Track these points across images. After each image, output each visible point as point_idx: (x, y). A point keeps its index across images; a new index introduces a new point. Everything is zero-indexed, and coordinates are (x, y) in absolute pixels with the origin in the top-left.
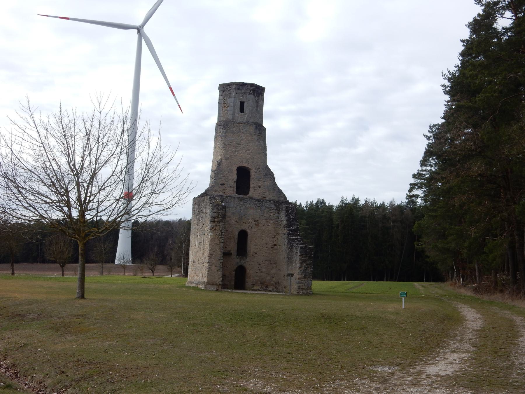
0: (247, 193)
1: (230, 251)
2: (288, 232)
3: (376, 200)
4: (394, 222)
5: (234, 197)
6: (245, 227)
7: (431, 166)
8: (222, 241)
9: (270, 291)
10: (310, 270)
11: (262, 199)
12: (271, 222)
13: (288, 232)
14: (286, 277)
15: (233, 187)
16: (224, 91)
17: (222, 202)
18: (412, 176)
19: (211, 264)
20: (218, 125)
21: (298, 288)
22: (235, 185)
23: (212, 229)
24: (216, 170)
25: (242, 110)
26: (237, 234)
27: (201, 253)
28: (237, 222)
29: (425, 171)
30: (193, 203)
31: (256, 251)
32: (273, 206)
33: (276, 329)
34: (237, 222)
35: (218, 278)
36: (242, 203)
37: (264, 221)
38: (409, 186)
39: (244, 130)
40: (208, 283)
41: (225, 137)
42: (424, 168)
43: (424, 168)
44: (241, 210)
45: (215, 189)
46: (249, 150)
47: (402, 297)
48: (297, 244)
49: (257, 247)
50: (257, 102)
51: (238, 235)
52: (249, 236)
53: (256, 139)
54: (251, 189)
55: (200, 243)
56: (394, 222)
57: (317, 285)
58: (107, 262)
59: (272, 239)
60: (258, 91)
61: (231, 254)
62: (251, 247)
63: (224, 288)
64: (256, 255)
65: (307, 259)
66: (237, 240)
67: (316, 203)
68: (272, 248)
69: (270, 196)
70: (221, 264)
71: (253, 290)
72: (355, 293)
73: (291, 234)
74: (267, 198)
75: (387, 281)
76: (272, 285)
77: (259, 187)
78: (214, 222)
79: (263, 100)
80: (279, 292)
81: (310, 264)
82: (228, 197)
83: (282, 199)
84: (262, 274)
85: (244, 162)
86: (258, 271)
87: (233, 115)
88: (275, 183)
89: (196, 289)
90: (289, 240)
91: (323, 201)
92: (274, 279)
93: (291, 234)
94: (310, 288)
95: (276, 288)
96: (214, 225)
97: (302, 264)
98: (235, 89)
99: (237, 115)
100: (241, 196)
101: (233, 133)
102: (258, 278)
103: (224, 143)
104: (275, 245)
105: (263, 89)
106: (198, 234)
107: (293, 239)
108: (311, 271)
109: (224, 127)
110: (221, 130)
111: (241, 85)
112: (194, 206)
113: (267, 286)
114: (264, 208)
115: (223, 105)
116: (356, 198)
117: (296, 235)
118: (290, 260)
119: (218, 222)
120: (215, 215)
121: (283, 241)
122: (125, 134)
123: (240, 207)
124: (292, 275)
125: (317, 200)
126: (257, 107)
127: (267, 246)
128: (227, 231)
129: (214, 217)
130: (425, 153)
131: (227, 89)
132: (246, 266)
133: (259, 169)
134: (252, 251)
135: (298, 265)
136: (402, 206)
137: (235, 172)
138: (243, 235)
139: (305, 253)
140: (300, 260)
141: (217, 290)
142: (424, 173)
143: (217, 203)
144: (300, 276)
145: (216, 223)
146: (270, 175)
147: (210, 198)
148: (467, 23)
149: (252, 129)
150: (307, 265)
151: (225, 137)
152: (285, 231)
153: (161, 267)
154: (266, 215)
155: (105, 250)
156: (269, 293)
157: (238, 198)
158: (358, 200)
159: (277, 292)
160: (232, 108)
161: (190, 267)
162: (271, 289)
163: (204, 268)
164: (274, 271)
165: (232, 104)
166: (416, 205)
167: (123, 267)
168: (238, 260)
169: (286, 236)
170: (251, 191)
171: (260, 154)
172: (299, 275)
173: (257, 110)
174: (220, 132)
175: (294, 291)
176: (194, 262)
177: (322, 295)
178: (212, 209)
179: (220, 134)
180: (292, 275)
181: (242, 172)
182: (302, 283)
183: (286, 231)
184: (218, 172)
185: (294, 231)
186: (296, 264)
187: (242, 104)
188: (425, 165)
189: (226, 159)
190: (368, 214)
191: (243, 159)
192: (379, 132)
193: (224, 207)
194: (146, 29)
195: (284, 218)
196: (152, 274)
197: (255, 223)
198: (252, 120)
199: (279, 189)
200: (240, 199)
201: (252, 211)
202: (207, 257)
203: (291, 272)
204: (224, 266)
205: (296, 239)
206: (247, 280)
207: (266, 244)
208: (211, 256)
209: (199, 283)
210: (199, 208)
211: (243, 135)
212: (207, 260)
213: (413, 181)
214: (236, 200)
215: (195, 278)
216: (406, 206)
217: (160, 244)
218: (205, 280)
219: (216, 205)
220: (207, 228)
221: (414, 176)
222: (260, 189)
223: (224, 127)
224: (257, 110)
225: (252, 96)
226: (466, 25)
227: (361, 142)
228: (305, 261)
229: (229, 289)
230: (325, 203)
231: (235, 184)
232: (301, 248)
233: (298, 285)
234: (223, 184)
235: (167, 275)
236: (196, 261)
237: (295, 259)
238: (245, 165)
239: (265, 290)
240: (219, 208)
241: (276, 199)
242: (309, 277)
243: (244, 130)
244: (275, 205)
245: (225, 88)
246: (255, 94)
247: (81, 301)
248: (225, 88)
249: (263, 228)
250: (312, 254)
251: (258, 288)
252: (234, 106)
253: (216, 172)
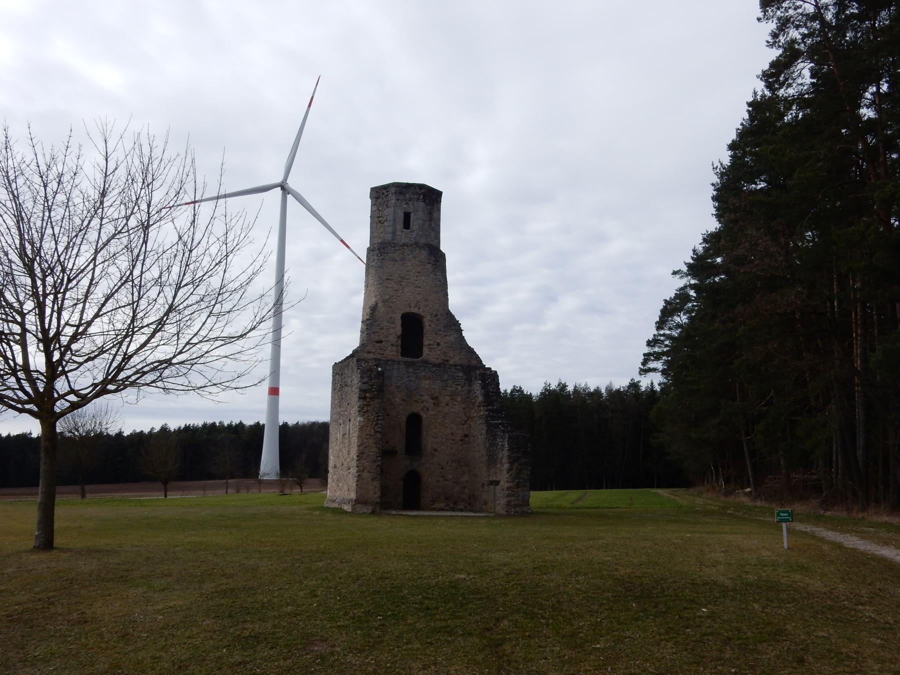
0: (420, 354)
3: (589, 385)
6: (416, 408)
7: (670, 329)
9: (461, 510)
12: (459, 399)
14: (486, 487)
16: (378, 198)
17: (378, 366)
18: (645, 343)
19: (361, 471)
21: (507, 505)
22: (400, 343)
23: (362, 411)
25: (407, 224)
26: (404, 419)
27: (345, 452)
28: (404, 400)
29: (664, 335)
32: (461, 374)
33: (507, 648)
34: (404, 400)
35: (374, 492)
36: (411, 370)
37: (448, 398)
39: (411, 256)
40: (358, 501)
41: (381, 267)
42: (662, 332)
43: (662, 332)
45: (367, 349)
47: (781, 521)
48: (503, 432)
51: (407, 422)
52: (425, 423)
54: (425, 349)
55: (344, 435)
57: (537, 498)
61: (396, 452)
62: (429, 441)
63: (386, 509)
66: (405, 430)
67: (512, 392)
69: (456, 358)
71: (433, 510)
72: (587, 508)
74: (451, 362)
77: (438, 344)
78: (365, 398)
79: (439, 210)
80: (476, 512)
82: (387, 361)
83: (474, 362)
85: (413, 305)
86: (441, 479)
87: (394, 233)
89: (339, 512)
90: (489, 426)
92: (466, 491)
94: (527, 503)
95: (470, 504)
96: (365, 403)
97: (511, 463)
98: (395, 193)
99: (400, 233)
100: (409, 360)
101: (394, 260)
104: (466, 436)
106: (341, 421)
109: (381, 253)
110: (375, 257)
112: (334, 376)
113: (455, 503)
115: (377, 220)
117: (499, 418)
118: (492, 460)
119: (371, 398)
120: (365, 387)
121: (479, 431)
123: (409, 377)
124: (497, 483)
128: (388, 415)
130: (662, 311)
134: (429, 446)
135: (506, 466)
138: (414, 422)
140: (509, 457)
141: (373, 512)
142: (662, 338)
148: (760, 73)
149: (424, 254)
151: (381, 267)
152: (482, 413)
153: (311, 481)
156: (460, 514)
157: (405, 362)
159: (472, 511)
160: (391, 223)
161: (330, 476)
162: (461, 507)
164: (465, 478)
165: (391, 217)
167: (270, 483)
170: (426, 351)
171: (437, 292)
172: (508, 482)
173: (430, 225)
175: (500, 509)
176: (335, 467)
177: (548, 514)
178: (361, 377)
180: (497, 483)
181: (409, 332)
184: (372, 322)
186: (502, 465)
187: (407, 216)
188: (662, 329)
189: (384, 301)
191: (410, 299)
192: (569, 302)
193: (381, 374)
194: (291, 183)
195: (478, 392)
198: (423, 241)
200: (408, 365)
201: (428, 382)
202: (355, 457)
205: (500, 424)
207: (452, 434)
208: (360, 456)
209: (343, 501)
211: (409, 264)
212: (354, 463)
213: (647, 350)
216: (627, 391)
217: (304, 448)
218: (353, 496)
219: (368, 371)
220: (354, 410)
221: (649, 343)
223: (380, 252)
224: (430, 225)
225: (422, 204)
226: (758, 77)
227: (575, 295)
229: (395, 509)
231: (400, 341)
232: (510, 438)
234: (381, 342)
236: (338, 465)
238: (415, 310)
239: (453, 510)
243: (411, 256)
245: (379, 194)
247: (44, 556)
248: (379, 194)
249: (447, 409)
251: (442, 505)
252: (394, 220)
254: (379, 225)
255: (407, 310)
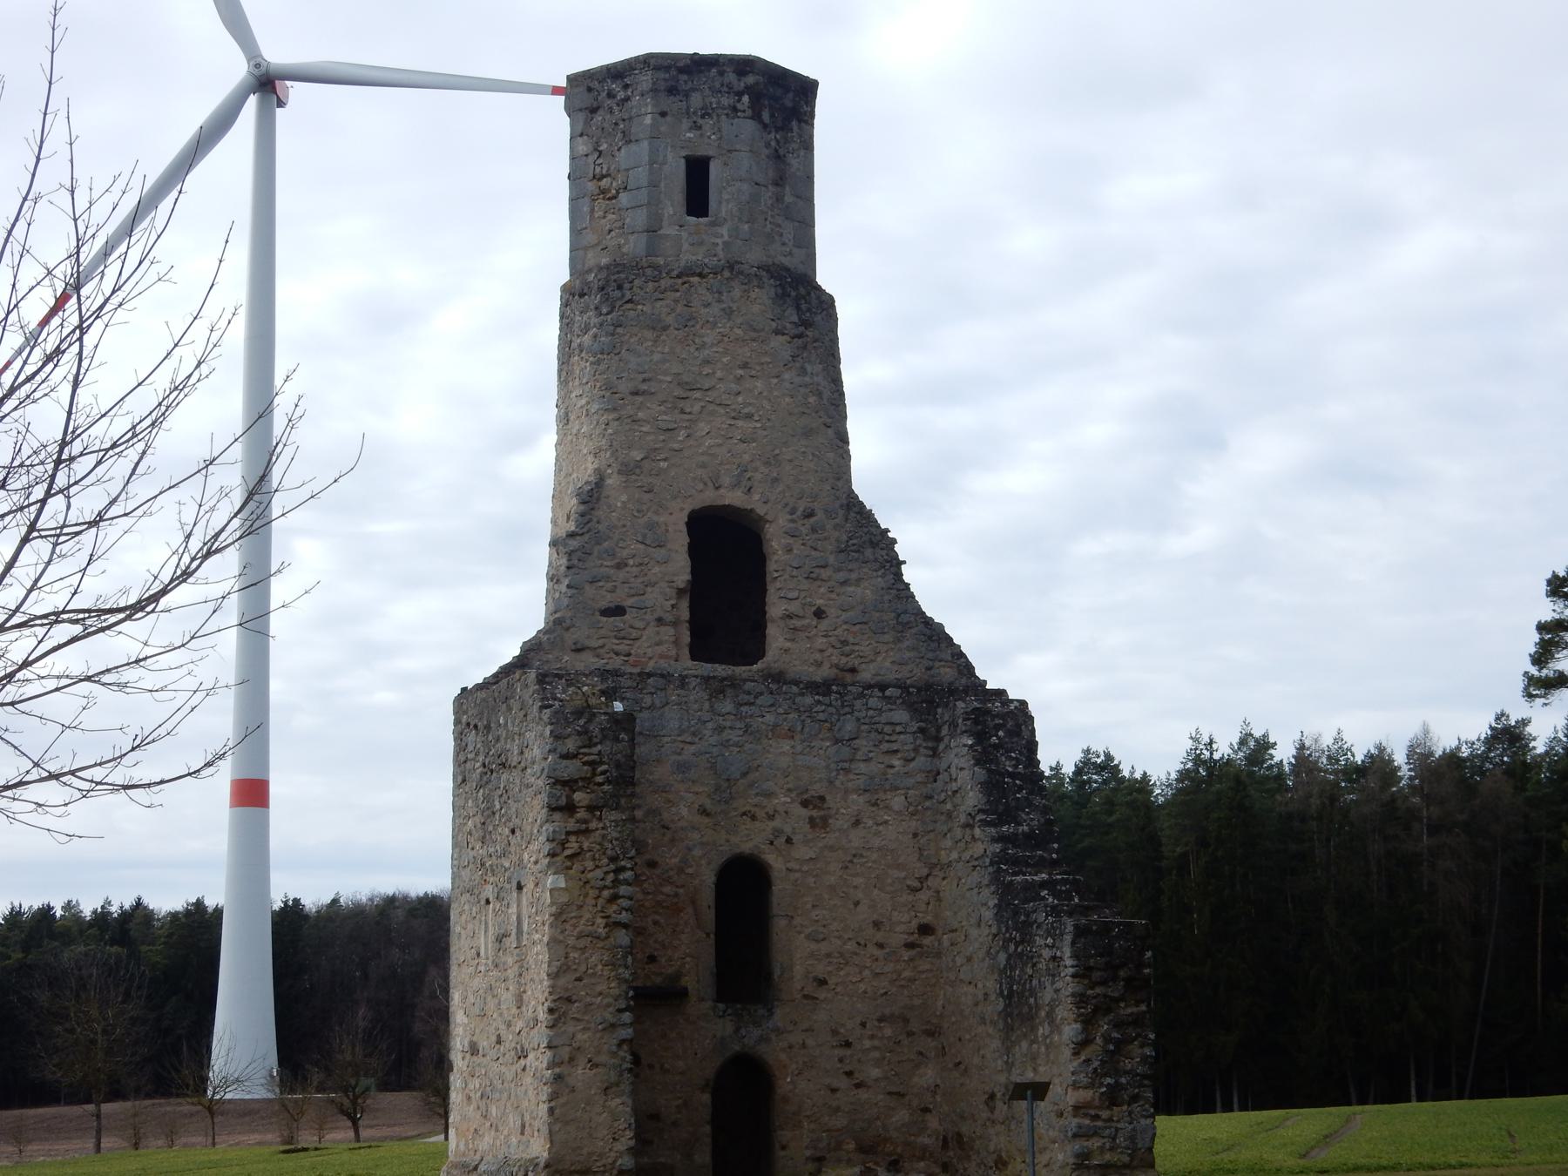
0: (755, 651)
1: (678, 976)
2: (997, 847)
3: (1349, 738)
4: (1434, 830)
5: (683, 678)
6: (751, 839)
8: (624, 917)
10: (1137, 1056)
11: (835, 681)
12: (898, 802)
13: (997, 847)
15: (675, 624)
16: (594, 110)
17: (610, 694)
18: (1544, 587)
20: (572, 295)
22: (685, 614)
23: (562, 853)
24: (571, 535)
25: (697, 201)
26: (709, 878)
27: (507, 997)
28: (704, 812)
30: (457, 722)
31: (820, 970)
32: (901, 715)
34: (704, 812)
36: (727, 706)
37: (858, 801)
38: (1536, 637)
39: (716, 309)
44: (725, 744)
45: (570, 637)
46: (749, 416)
48: (1054, 911)
49: (824, 948)
50: (778, 157)
52: (781, 889)
53: (786, 354)
54: (771, 630)
55: (500, 939)
56: (1434, 830)
58: (163, 1086)
59: (906, 897)
60: (777, 102)
61: (683, 994)
62: (797, 950)
64: (822, 994)
65: (1115, 991)
66: (710, 916)
67: (1079, 771)
68: (910, 946)
69: (884, 661)
70: (624, 1053)
73: (1014, 861)
74: (866, 675)
75: (1420, 1099)
76: (924, 1154)
77: (819, 614)
78: (570, 808)
81: (1136, 1021)
82: (645, 675)
83: (947, 674)
84: (863, 1095)
86: (843, 1083)
87: (652, 230)
88: (903, 592)
91: (1109, 757)
92: (933, 1122)
93: (1014, 861)
96: (572, 825)
97: (1087, 1022)
98: (654, 90)
100: (721, 670)
101: (659, 327)
102: (840, 1122)
103: (608, 387)
104: (925, 930)
105: (805, 89)
107: (1028, 886)
108: (1144, 1059)
109: (605, 297)
111: (681, 71)
114: (849, 727)
115: (591, 186)
116: (1257, 733)
117: (1041, 864)
118: (1018, 1010)
119: (591, 808)
120: (572, 769)
122: (50, 348)
123: (720, 729)
124: (1039, 1091)
125: (1079, 756)
126: (779, 181)
127: (879, 936)
128: (652, 864)
129: (569, 784)
131: (611, 95)
132: (774, 1053)
133: (809, 514)
134: (798, 970)
135: (1070, 1031)
136: (1464, 760)
137: (680, 541)
138: (744, 883)
139: (1102, 963)
140: (1080, 1000)
143: (579, 702)
144: (1086, 1095)
145: (581, 814)
146: (874, 545)
147: (542, 679)
149: (759, 302)
150: (1117, 1025)
151: (612, 350)
152: (978, 849)
154: (862, 767)
155: (105, 1032)
157: (706, 680)
158: (1264, 745)
160: (643, 196)
163: (528, 1080)
164: (928, 1075)
165: (641, 176)
166: (1526, 748)
168: (725, 1027)
169: (983, 876)
170: (776, 638)
171: (808, 433)
172: (1075, 1086)
173: (779, 199)
174: (586, 330)
176: (474, 1050)
178: (557, 737)
179: (587, 339)
180: (1039, 1091)
181: (718, 561)
182: (1096, 1133)
183: (983, 844)
184: (586, 543)
185: (1031, 840)
186: (1055, 1027)
187: (697, 170)
189: (628, 470)
190: (1315, 802)
191: (716, 462)
194: (277, 54)
196: (351, 1134)
197: (805, 812)
198: (754, 256)
199: (928, 622)
200: (717, 688)
201: (786, 746)
202: (542, 1015)
203: (1030, 1076)
204: (639, 1063)
205: (1043, 885)
206: (784, 1135)
207: (877, 925)
208: (560, 1009)
210: (486, 743)
211: (710, 336)
212: (540, 1036)
213: (1548, 610)
214: (697, 694)
215: (485, 1143)
216: (1484, 757)
219: (578, 713)
220: (534, 850)
222: (824, 625)
223: (606, 298)
224: (779, 199)
225: (748, 127)
228: (1104, 1007)
230: (1116, 769)
231: (685, 604)
232: (1080, 932)
233: (1077, 1146)
234: (619, 611)
235: (430, 1134)
236: (483, 1044)
237: (1047, 995)
240: (595, 729)
241: (915, 673)
242: (1135, 1098)
243: (716, 309)
244: (911, 707)
246: (766, 116)
249: (856, 839)
250: (1140, 965)
252: (653, 185)
253: (574, 544)
254: (601, 204)
255: (709, 498)
